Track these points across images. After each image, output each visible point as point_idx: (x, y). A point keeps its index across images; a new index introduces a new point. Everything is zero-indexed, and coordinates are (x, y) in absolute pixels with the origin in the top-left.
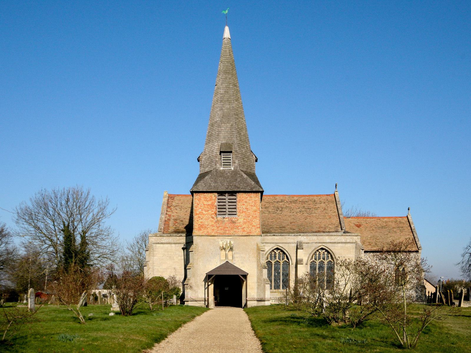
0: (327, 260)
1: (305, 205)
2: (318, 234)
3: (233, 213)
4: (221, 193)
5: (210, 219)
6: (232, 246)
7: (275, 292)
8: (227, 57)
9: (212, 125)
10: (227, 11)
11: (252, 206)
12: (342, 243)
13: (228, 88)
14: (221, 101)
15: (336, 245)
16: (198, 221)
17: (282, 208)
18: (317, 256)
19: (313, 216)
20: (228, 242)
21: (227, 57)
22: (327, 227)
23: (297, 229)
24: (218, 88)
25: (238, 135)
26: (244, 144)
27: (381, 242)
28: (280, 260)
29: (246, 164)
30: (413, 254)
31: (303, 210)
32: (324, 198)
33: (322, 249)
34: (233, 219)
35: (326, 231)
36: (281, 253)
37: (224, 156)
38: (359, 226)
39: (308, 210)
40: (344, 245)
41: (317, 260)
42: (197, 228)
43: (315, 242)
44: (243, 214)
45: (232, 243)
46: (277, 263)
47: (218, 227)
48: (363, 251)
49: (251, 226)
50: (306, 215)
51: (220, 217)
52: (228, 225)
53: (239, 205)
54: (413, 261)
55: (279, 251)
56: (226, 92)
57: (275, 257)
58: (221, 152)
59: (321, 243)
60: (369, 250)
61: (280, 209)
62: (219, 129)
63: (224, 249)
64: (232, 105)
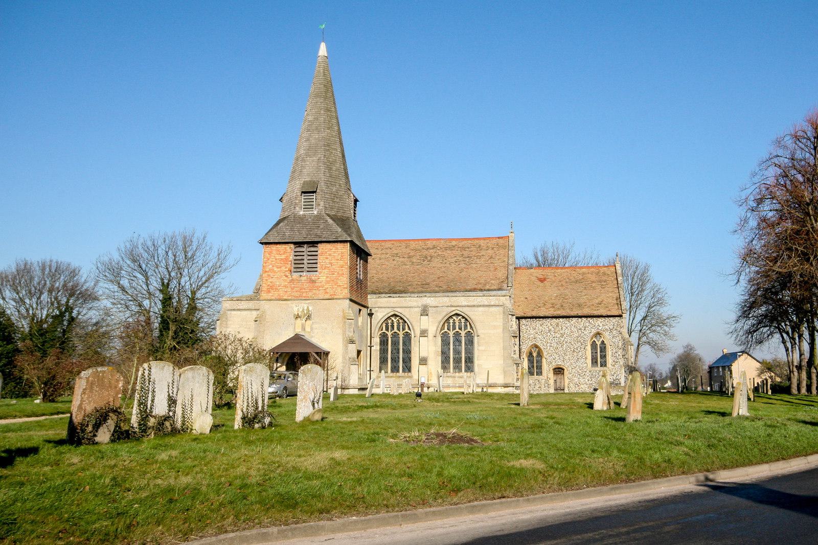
0: (465, 330)
1: (464, 253)
2: (450, 294)
3: (313, 269)
4: (299, 244)
5: (282, 278)
6: (310, 312)
7: (392, 377)
8: (321, 77)
9: (297, 159)
10: (324, 26)
11: (337, 260)
12: (484, 306)
13: (318, 115)
14: (308, 130)
15: (476, 309)
16: (267, 280)
17: (431, 257)
18: (451, 324)
19: (472, 267)
20: (306, 308)
21: (321, 77)
22: (488, 282)
23: (445, 287)
24: (308, 115)
25: (327, 171)
26: (336, 181)
27: (570, 303)
28: (400, 331)
29: (337, 205)
30: (615, 320)
31: (461, 259)
32: (494, 241)
33: (457, 315)
34: (313, 278)
35: (485, 288)
36: (401, 321)
37: (305, 197)
38: (542, 280)
39: (467, 260)
40: (486, 309)
41: (463, 330)
42: (265, 289)
43: (447, 305)
44: (326, 271)
45: (310, 308)
46: (395, 335)
47: (292, 289)
48: (514, 317)
49: (336, 286)
50: (463, 266)
51: (296, 275)
52: (306, 285)
53: (320, 259)
54: (616, 330)
55: (398, 318)
56: (316, 119)
57: (393, 326)
58: (303, 192)
59: (455, 306)
60: (549, 315)
61: (429, 258)
62: (303, 163)
63: (297, 317)
64: (322, 134)
